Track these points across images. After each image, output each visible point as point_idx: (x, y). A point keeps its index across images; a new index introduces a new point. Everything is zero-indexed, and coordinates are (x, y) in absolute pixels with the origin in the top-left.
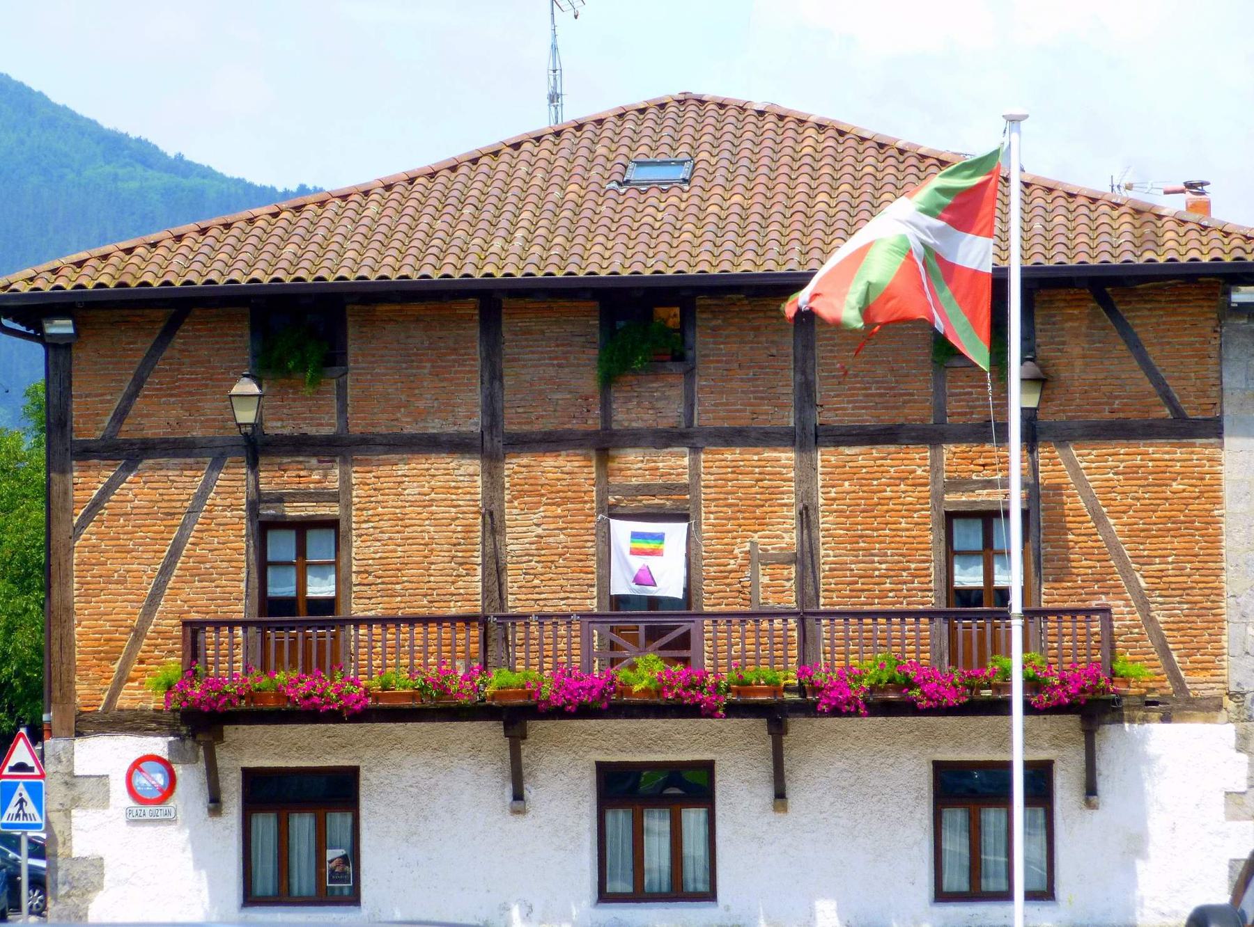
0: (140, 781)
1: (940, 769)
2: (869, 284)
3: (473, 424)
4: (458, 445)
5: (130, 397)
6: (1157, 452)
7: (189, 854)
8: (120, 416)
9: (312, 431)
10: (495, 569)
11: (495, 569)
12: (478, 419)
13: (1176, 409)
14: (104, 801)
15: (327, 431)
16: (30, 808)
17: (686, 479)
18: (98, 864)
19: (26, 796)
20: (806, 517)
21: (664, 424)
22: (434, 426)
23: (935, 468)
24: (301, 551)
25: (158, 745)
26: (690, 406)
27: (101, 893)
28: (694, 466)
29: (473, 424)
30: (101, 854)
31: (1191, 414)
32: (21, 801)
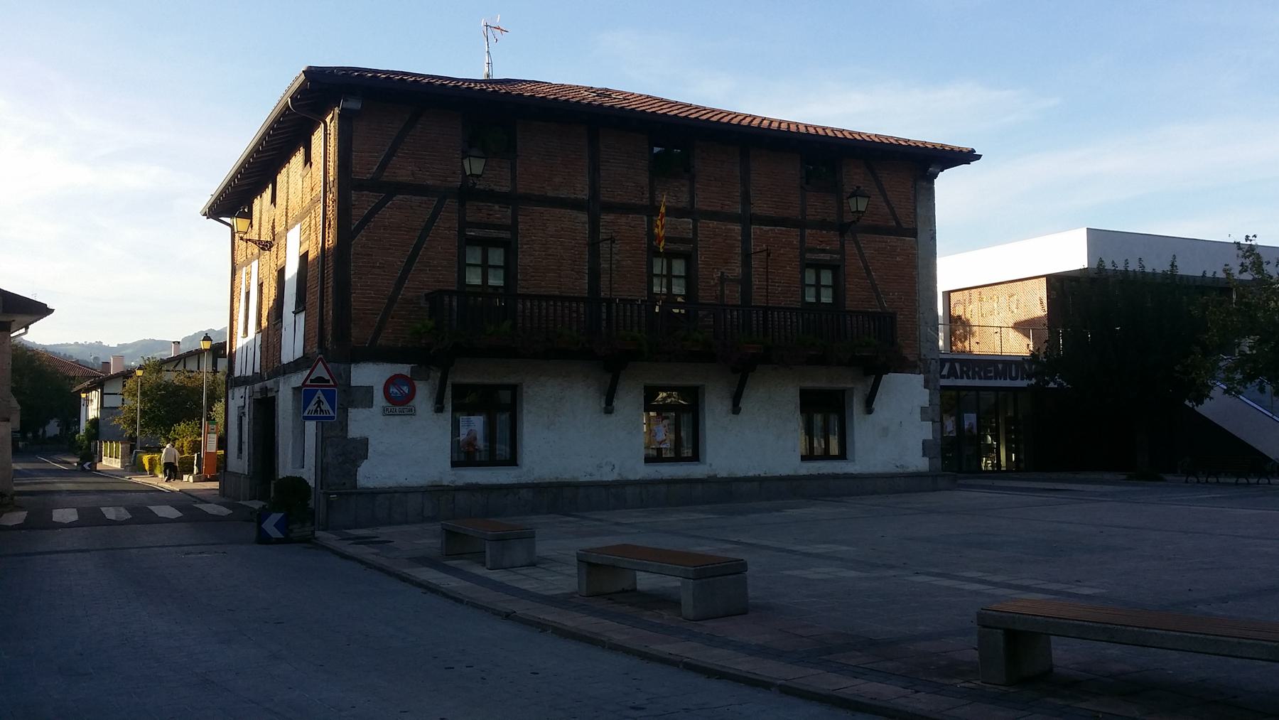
0: (393, 390)
1: (804, 393)
2: (739, 567)
3: (584, 195)
4: (575, 205)
5: (389, 157)
6: (892, 240)
7: (1134, 266)
8: (383, 166)
9: (497, 188)
10: (595, 275)
11: (595, 275)
12: (587, 192)
13: (898, 223)
14: (369, 404)
15: (504, 189)
16: (326, 406)
17: (691, 236)
18: (364, 442)
19: (322, 398)
20: (747, 257)
21: (680, 205)
22: (563, 193)
23: (802, 240)
24: (485, 258)
25: (404, 369)
26: (692, 198)
27: (899, 318)
28: (695, 227)
29: (584, 195)
30: (365, 433)
31: (905, 226)
32: (319, 402)
